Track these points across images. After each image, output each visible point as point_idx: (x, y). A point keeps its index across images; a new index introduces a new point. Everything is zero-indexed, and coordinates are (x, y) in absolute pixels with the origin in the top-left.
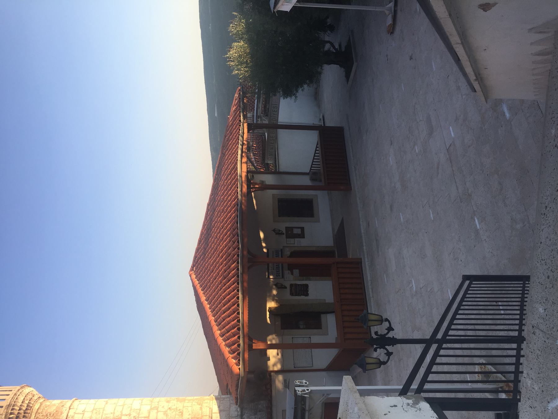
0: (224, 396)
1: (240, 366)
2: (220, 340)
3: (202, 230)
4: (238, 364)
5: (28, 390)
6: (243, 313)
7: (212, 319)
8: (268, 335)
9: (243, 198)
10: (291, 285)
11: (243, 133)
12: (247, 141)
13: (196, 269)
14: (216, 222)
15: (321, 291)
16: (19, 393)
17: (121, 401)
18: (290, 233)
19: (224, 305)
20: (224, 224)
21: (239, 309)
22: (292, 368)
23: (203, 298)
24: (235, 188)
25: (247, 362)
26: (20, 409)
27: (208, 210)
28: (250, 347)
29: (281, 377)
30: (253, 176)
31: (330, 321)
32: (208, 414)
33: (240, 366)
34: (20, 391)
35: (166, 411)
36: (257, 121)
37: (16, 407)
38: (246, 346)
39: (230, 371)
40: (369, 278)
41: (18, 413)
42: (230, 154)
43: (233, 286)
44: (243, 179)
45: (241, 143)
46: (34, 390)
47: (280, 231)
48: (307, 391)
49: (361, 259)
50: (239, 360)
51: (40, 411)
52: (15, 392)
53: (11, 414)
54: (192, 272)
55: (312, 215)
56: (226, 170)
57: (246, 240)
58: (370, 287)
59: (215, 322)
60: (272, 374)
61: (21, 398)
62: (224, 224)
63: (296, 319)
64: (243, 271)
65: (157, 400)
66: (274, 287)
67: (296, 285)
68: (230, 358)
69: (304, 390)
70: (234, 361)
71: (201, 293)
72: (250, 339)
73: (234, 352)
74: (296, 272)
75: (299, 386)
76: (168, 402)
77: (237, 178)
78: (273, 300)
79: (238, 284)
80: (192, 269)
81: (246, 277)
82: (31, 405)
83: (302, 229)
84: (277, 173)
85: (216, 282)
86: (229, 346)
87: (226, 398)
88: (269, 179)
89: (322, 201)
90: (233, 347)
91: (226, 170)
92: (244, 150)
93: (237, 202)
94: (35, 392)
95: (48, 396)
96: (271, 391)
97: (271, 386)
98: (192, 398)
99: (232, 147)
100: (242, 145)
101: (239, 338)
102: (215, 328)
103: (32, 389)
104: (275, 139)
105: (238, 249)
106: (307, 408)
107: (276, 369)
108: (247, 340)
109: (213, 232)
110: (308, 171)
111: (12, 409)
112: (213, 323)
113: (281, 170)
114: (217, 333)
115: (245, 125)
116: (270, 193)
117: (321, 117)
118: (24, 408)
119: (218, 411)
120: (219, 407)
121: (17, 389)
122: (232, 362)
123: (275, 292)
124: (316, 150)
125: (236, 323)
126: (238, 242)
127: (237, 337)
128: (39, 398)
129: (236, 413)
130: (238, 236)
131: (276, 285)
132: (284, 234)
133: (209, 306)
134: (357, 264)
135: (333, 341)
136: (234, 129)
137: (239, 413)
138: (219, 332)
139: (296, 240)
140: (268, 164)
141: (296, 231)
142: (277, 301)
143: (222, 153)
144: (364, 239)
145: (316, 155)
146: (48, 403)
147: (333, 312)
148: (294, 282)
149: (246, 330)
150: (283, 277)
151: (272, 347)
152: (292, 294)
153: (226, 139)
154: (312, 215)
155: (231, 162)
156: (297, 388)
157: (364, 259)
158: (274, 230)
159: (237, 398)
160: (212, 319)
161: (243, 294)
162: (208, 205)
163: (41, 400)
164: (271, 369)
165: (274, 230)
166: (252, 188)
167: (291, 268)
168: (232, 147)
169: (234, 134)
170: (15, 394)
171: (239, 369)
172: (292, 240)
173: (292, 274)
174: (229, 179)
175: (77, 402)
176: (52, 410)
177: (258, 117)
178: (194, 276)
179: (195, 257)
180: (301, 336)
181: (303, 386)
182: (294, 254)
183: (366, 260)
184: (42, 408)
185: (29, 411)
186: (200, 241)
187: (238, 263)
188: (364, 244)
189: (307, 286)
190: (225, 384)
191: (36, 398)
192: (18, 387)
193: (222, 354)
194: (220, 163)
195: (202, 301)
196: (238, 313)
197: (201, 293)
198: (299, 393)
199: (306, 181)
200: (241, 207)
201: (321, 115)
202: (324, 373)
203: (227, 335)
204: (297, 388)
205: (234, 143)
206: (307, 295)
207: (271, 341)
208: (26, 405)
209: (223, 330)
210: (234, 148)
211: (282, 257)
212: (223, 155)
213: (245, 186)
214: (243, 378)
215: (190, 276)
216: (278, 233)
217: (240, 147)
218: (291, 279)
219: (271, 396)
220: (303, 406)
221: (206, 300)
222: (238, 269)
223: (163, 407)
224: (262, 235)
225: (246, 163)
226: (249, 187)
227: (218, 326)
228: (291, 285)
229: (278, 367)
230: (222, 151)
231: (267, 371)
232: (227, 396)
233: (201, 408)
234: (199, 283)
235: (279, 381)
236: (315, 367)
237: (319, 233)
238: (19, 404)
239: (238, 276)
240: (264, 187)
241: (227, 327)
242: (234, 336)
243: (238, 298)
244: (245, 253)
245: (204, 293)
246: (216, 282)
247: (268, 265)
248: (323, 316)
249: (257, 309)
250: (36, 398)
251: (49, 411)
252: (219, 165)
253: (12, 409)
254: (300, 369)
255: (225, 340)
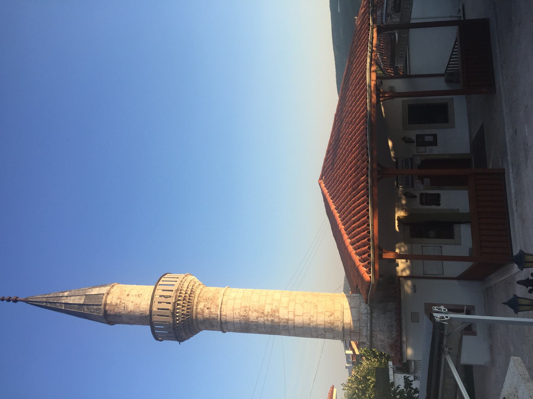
0: (354, 295)
1: (371, 275)
2: (351, 248)
3: (330, 140)
4: (369, 272)
5: (190, 278)
6: (373, 225)
7: (342, 227)
8: (397, 243)
9: (373, 109)
10: (422, 195)
11: (373, 38)
12: (376, 47)
13: (325, 178)
14: (344, 134)
15: (455, 200)
16: (184, 280)
17: (264, 292)
18: (421, 141)
19: (354, 216)
20: (353, 136)
21: (369, 222)
22: (422, 275)
23: (333, 207)
24: (364, 99)
25: (378, 274)
26: (186, 293)
27: (335, 121)
28: (380, 256)
29: (409, 283)
30: (381, 82)
31: (465, 232)
32: (340, 309)
33: (371, 275)
34: (185, 278)
35: (303, 304)
36: (386, 20)
37: (182, 292)
38: (377, 256)
39: (362, 278)
40: (513, 191)
41: (185, 296)
42: (358, 62)
43: (362, 199)
44: (372, 89)
45: (370, 50)
46: (195, 278)
47: (410, 139)
48: (446, 319)
49: (504, 169)
50: (370, 269)
51: (201, 295)
52: (181, 279)
53: (179, 296)
54: (321, 181)
55: (446, 121)
56: (354, 79)
57: (375, 153)
58: (514, 200)
59: (346, 230)
60: (401, 279)
61: (186, 285)
62: (353, 136)
63: (425, 228)
64: (372, 183)
65: (294, 293)
66: (403, 197)
67: (427, 194)
68: (361, 266)
69: (443, 317)
70: (365, 269)
71: (330, 201)
72: (380, 250)
73: (364, 261)
74: (427, 181)
75: (437, 312)
76: (304, 295)
77: (366, 88)
78: (402, 209)
79: (368, 197)
80: (321, 178)
81: (376, 190)
82: (194, 290)
83: (435, 136)
84: (407, 76)
85: (346, 193)
86: (359, 254)
87: (356, 297)
88: (399, 85)
89: (459, 107)
90: (363, 256)
91: (354, 79)
92: (373, 57)
93: (366, 113)
94: (196, 280)
95: (207, 284)
96: (400, 294)
97: (400, 290)
98: (325, 294)
99: (360, 55)
100: (371, 53)
101: (369, 248)
102: (345, 237)
103: (193, 277)
104: (405, 41)
105: (368, 162)
106: (446, 333)
107: (404, 274)
108: (377, 252)
109: (341, 144)
110: (443, 72)
111: (180, 293)
112: (343, 232)
113: (412, 73)
114: (348, 241)
115: (375, 30)
116: (399, 101)
117: (461, 7)
118: (189, 293)
119: (349, 308)
120: (350, 304)
121: (182, 277)
122: (363, 270)
123: (404, 202)
124: (454, 48)
125: (366, 234)
126: (367, 155)
127: (367, 247)
128: (200, 284)
129: (366, 311)
130: (367, 149)
131: (405, 195)
132: (414, 142)
133: (338, 215)
134: (499, 176)
135: (466, 253)
136: (363, 34)
137: (369, 311)
138: (349, 240)
139: (428, 148)
140: (397, 67)
141: (427, 139)
142: (406, 211)
143: (349, 61)
144: (508, 147)
145: (454, 53)
146: (207, 289)
147: (469, 222)
148: (424, 192)
149: (376, 242)
150: (413, 186)
151: (401, 257)
152: (422, 203)
153: (354, 46)
154: (446, 121)
155: (359, 71)
156: (435, 314)
157: (509, 170)
158: (404, 139)
159: (367, 300)
160: (342, 227)
161: (373, 207)
162: (336, 115)
163: (201, 287)
164: (400, 274)
165: (404, 139)
166: (381, 97)
167: (421, 178)
168: (360, 55)
169: (363, 39)
170: (181, 281)
171: (370, 277)
172: (423, 149)
173: (423, 184)
174: (357, 90)
175: (229, 290)
176: (210, 295)
177: (387, 15)
178: (323, 185)
179: (324, 167)
180: (431, 246)
181: (441, 313)
182: (362, 15)
183: (511, 171)
184: (202, 293)
185: (192, 295)
186: (328, 152)
187: (367, 176)
188: (509, 154)
189: (438, 195)
190: (355, 284)
191: (197, 284)
192: (183, 275)
193: (346, 248)
194: (347, 71)
195: (332, 209)
196: (368, 225)
197: (330, 201)
198: (438, 320)
199: (441, 85)
200: (370, 119)
201: (461, 5)
202: (456, 282)
203: (358, 244)
204: (435, 314)
205: (363, 50)
206: (439, 204)
207: (400, 249)
208: (190, 290)
209: (353, 240)
210: (362, 56)
211: (412, 168)
212: (351, 63)
213: (374, 96)
214: (373, 285)
215: (320, 185)
216: (408, 141)
217: (369, 54)
218: (420, 189)
219: (400, 299)
220: (442, 332)
221: (336, 209)
222: (367, 183)
223: (300, 300)
224: (390, 144)
225: (375, 71)
226: (378, 97)
227: (337, 210)
228: (422, 195)
229: (407, 273)
230: (350, 59)
231: (396, 276)
232: (357, 295)
233: (333, 304)
234: (328, 192)
235: (408, 285)
236: (445, 275)
237: (454, 139)
238: (185, 289)
239: (368, 190)
240: (394, 95)
241: (357, 237)
242: (364, 246)
243: (368, 210)
244: (375, 165)
245: (333, 202)
246: (346, 193)
247: (397, 177)
248: (456, 227)
249: (386, 221)
250: (197, 284)
251: (208, 296)
252: (346, 74)
253: (180, 293)
254: (428, 276)
255: (355, 249)
